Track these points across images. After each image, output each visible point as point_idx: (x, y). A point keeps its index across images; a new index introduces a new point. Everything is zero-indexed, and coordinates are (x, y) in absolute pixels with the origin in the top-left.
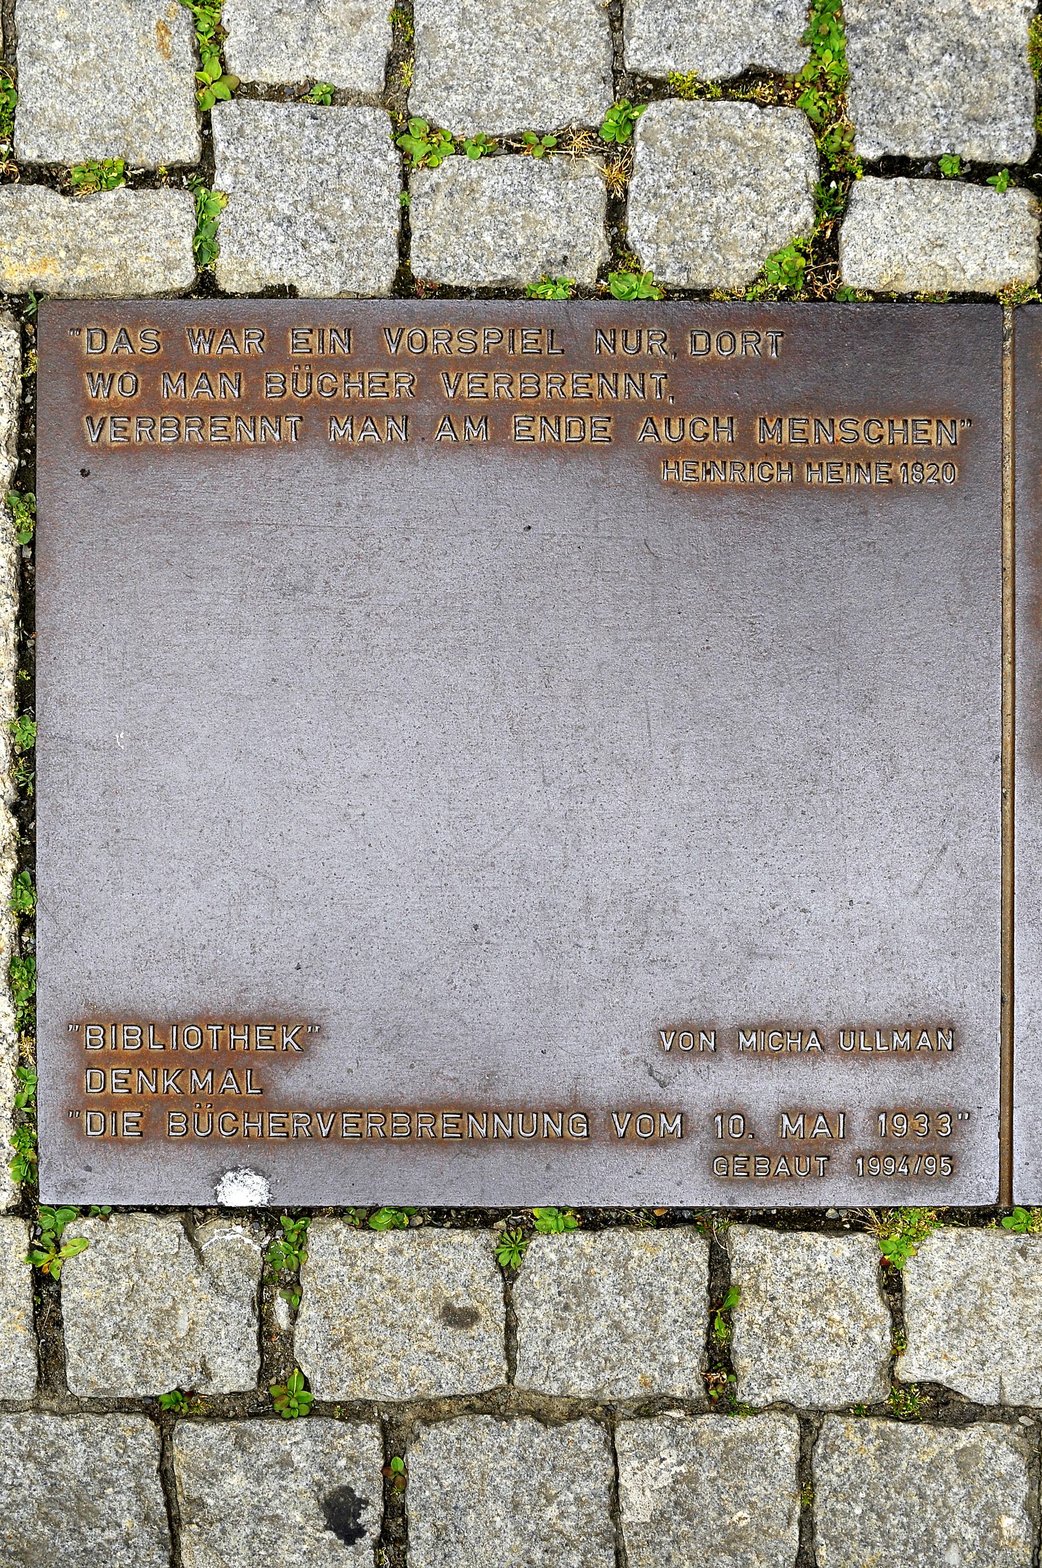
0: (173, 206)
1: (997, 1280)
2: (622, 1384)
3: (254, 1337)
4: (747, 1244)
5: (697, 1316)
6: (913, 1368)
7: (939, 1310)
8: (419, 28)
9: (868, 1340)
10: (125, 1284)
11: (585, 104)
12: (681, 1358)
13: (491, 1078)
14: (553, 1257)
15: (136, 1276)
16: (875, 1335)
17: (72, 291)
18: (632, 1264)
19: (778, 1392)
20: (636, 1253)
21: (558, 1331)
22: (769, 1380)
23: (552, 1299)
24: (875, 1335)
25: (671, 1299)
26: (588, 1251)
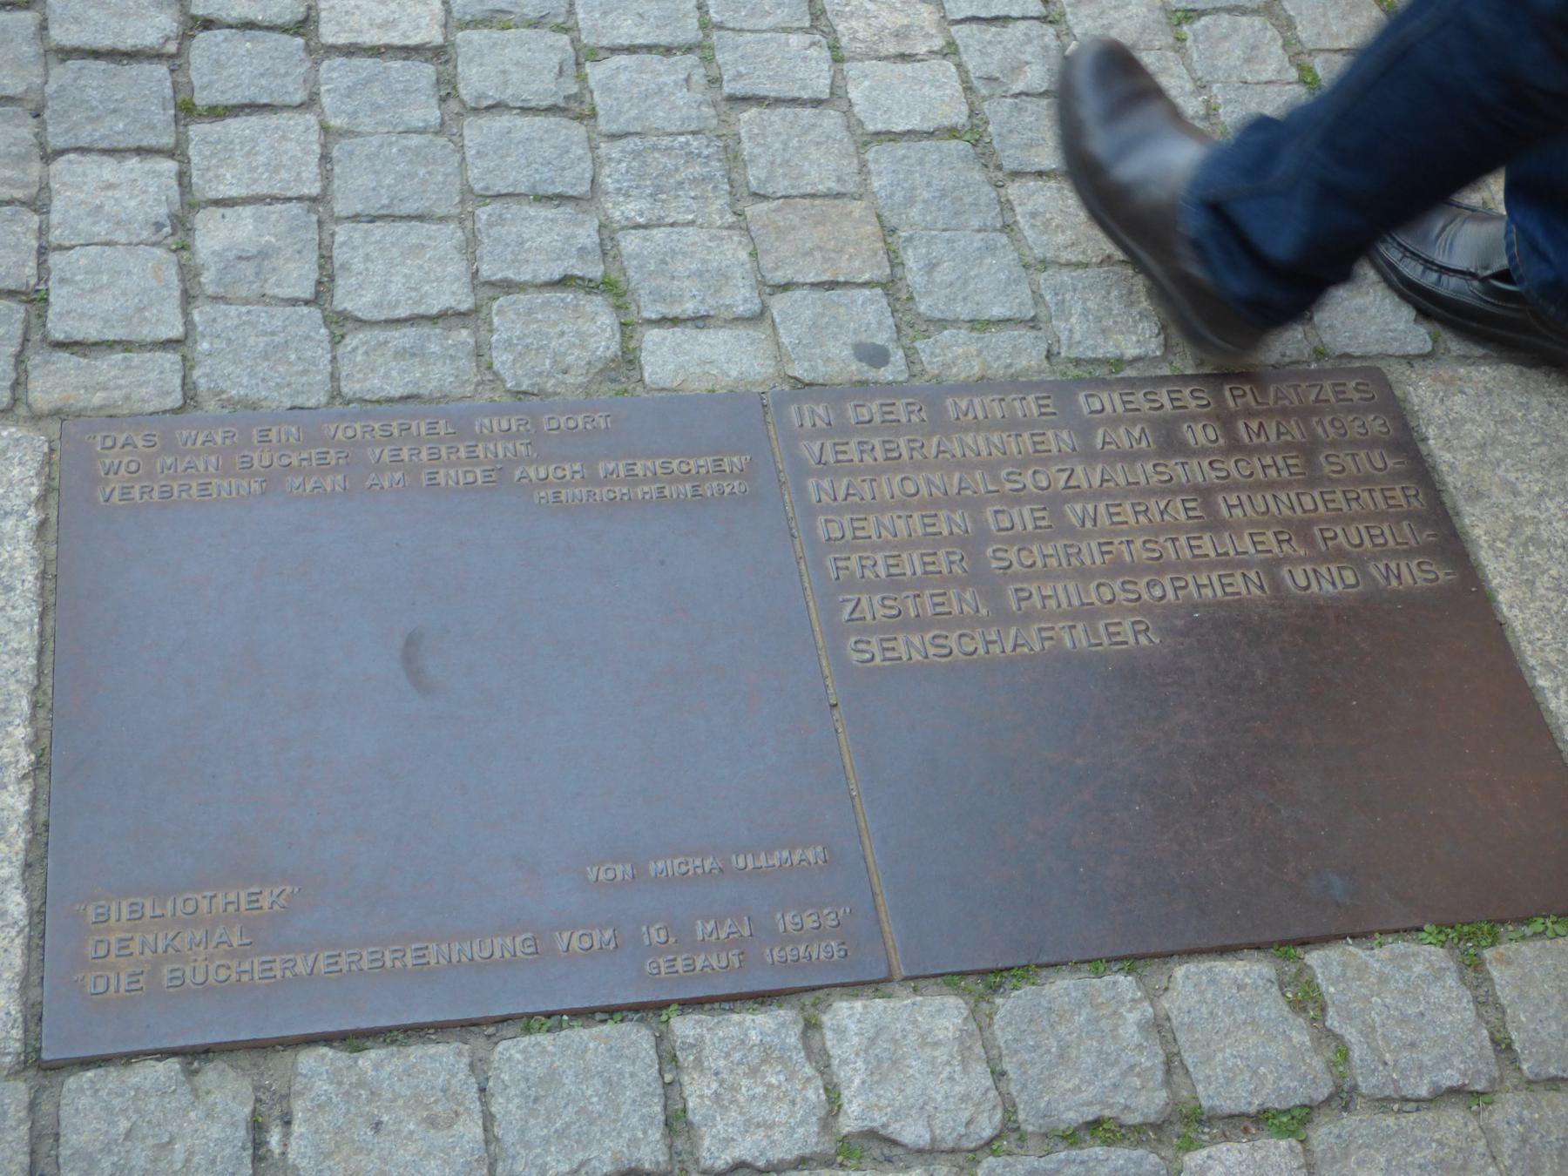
0: (171, 359)
1: (904, 1037)
2: (595, 1163)
3: (248, 1161)
4: (685, 1027)
5: (653, 1095)
6: (852, 1119)
7: (860, 1064)
8: (337, 265)
9: (806, 1099)
10: (124, 1125)
11: (451, 294)
12: (645, 1133)
13: (191, 1073)
14: (519, 1056)
15: (134, 1117)
16: (811, 1094)
17: (1446, 498)
18: (589, 1055)
19: (737, 1153)
20: (591, 1045)
21: (532, 1122)
22: (728, 1141)
23: (522, 1093)
24: (811, 1094)
25: (627, 1082)
26: (550, 1048)
